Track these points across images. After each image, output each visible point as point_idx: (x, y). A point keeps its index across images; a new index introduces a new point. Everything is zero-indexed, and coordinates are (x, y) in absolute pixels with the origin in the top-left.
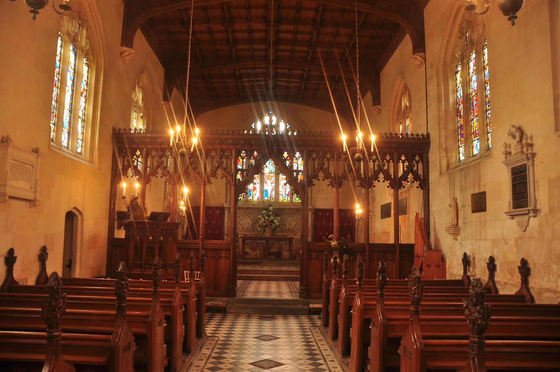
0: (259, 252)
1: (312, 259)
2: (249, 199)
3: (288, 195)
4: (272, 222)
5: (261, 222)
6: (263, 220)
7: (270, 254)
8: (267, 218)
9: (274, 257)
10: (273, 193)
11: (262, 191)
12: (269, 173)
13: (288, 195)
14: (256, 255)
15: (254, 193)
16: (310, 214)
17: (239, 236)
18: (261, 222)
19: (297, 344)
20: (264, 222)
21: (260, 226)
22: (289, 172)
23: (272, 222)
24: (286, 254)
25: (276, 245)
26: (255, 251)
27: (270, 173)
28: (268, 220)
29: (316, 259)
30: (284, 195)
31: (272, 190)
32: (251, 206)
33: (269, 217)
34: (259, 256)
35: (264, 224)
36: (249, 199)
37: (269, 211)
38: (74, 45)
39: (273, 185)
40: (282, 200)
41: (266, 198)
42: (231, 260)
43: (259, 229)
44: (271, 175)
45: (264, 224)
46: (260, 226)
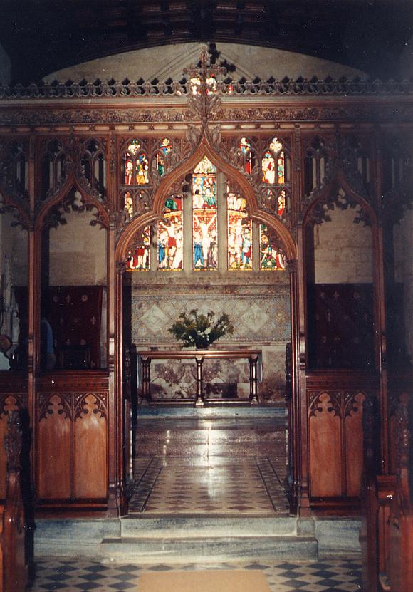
0: (186, 385)
1: (86, 412)
3: (248, 255)
7: (211, 389)
9: (220, 395)
12: (204, 206)
13: (248, 255)
14: (180, 393)
15: (172, 252)
17: (219, 58)
22: (251, 188)
24: (245, 387)
25: (224, 368)
26: (177, 382)
29: (95, 411)
30: (238, 256)
31: (212, 244)
34: (185, 395)
38: (207, 497)
39: (214, 233)
42: (112, 421)
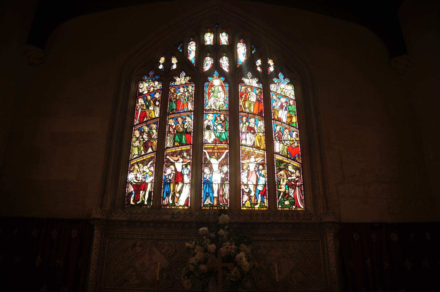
2: (165, 202)
4: (230, 259)
5: (193, 260)
6: (199, 255)
8: (212, 247)
10: (227, 189)
11: (199, 184)
12: (215, 142)
13: (263, 193)
16: (330, 237)
18: (193, 260)
19: (216, 174)
20: (205, 261)
21: (189, 274)
23: (230, 259)
27: (218, 141)
28: (216, 253)
31: (223, 180)
32: (167, 217)
33: (219, 246)
35: (203, 267)
36: (165, 202)
37: (220, 226)
39: (226, 169)
40: (248, 204)
41: (208, 202)
43: (187, 283)
44: (220, 146)
45: (203, 267)
46: (189, 274)
